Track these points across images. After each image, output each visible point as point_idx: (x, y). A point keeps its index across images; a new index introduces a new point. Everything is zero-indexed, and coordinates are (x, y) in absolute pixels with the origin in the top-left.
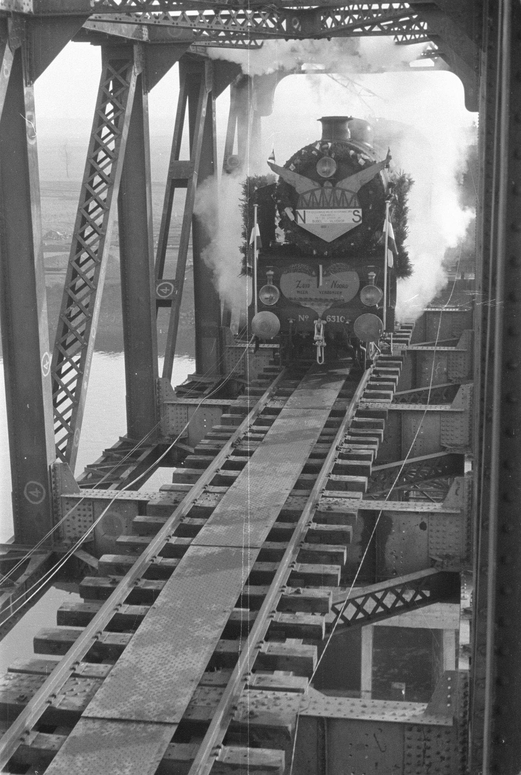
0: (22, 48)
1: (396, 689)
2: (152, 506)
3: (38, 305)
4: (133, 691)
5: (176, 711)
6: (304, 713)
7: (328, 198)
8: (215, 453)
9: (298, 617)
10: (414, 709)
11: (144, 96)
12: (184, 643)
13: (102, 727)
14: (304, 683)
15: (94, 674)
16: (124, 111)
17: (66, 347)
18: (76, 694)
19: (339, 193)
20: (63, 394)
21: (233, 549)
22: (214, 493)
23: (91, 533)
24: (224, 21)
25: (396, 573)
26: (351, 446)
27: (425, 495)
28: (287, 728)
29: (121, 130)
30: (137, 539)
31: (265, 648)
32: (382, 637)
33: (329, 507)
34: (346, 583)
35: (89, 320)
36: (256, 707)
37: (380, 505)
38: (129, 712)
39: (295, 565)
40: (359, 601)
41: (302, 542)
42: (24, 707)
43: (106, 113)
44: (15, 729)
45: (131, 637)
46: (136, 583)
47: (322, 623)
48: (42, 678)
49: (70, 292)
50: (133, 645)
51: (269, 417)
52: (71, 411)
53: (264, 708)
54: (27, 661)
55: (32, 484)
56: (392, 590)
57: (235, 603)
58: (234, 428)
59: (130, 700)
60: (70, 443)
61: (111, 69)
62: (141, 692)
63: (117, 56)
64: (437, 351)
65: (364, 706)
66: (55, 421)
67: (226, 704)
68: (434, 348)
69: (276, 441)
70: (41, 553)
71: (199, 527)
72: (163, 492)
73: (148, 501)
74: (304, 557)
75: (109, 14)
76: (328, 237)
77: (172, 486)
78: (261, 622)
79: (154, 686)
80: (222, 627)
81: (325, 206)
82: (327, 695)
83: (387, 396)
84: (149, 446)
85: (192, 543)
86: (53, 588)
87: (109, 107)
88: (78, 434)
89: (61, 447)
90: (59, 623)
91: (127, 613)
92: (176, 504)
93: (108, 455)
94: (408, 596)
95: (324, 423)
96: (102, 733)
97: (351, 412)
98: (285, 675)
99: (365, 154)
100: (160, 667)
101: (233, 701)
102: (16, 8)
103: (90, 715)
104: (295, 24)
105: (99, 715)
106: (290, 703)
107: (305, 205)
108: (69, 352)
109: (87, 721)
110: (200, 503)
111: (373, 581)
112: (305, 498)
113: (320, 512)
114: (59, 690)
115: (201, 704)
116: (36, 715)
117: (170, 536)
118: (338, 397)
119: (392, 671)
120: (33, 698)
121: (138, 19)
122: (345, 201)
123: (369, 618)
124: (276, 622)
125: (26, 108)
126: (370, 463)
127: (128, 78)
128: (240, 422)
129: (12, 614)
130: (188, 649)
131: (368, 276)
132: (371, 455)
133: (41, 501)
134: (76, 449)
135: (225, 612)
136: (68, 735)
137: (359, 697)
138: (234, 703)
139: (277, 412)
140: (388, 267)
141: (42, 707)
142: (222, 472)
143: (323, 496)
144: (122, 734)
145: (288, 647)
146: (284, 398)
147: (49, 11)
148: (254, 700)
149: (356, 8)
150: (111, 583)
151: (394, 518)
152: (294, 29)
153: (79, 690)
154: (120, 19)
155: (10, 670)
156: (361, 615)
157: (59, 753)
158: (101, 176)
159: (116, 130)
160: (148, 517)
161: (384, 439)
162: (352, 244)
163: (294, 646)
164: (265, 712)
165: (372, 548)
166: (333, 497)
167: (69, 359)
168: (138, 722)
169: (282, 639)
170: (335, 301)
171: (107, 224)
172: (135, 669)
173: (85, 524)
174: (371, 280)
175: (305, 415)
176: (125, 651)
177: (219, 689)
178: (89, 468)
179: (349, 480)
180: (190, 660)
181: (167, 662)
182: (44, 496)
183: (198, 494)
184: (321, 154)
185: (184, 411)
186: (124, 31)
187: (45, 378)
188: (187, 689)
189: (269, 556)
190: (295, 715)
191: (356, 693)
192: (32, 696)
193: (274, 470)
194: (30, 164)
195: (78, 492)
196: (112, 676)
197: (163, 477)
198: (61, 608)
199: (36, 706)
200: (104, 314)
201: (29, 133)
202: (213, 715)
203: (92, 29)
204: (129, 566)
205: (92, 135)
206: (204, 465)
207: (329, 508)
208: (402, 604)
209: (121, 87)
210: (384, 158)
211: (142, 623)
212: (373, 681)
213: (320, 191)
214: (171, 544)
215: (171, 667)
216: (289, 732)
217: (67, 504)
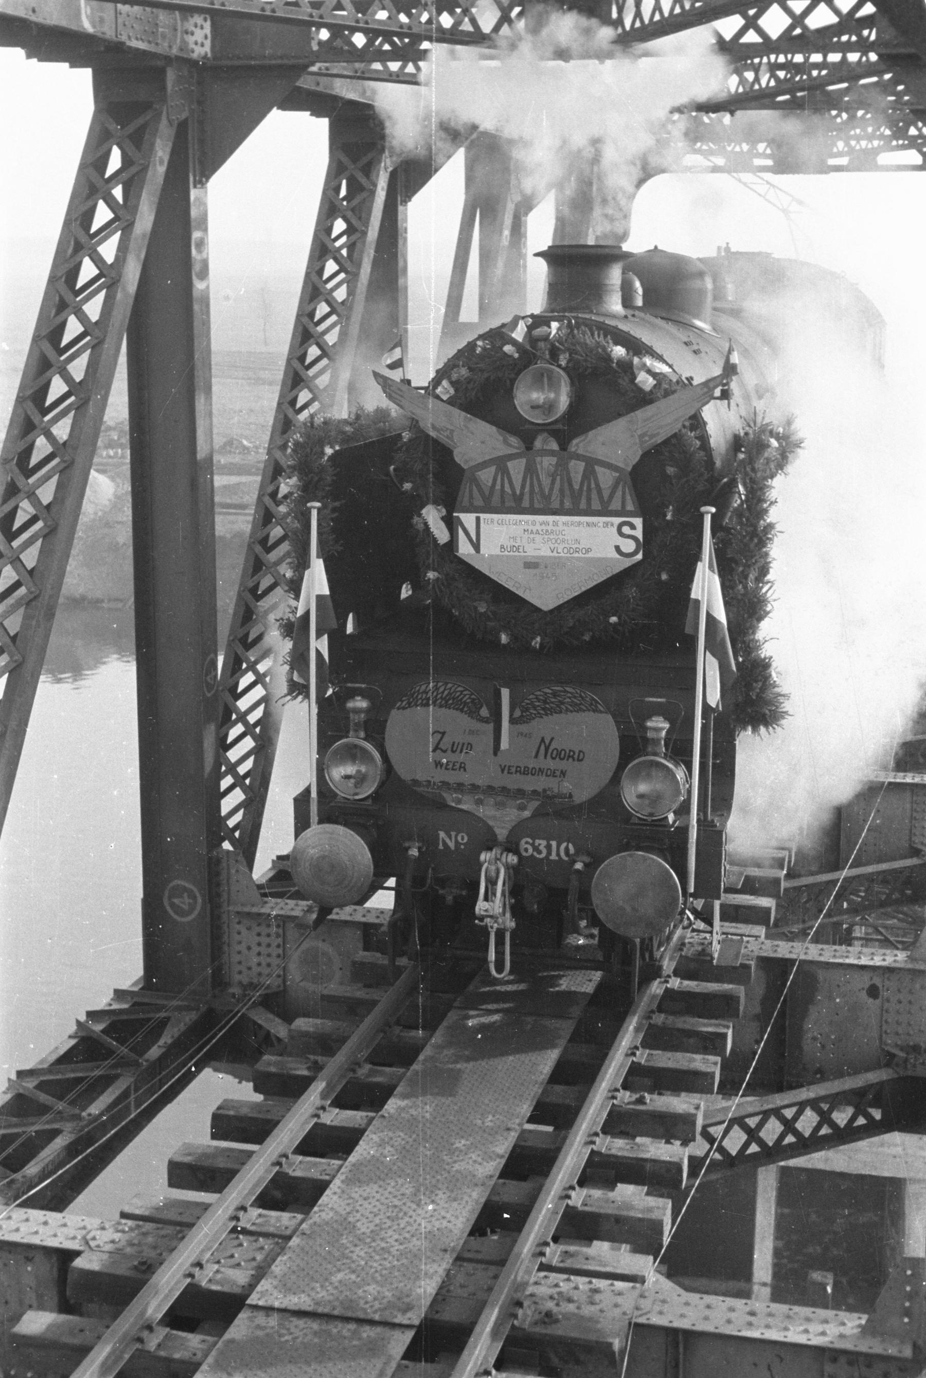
0: (190, 122)
1: (814, 1283)
7: (546, 481)
9: (638, 1145)
10: (844, 1324)
11: (400, 208)
12: (434, 1181)
14: (646, 1265)
15: (271, 1230)
16: (365, 233)
18: (239, 1265)
19: (577, 468)
25: (821, 1075)
27: (881, 934)
28: (610, 1345)
29: (359, 266)
31: (578, 1198)
32: (792, 1188)
33: (703, 950)
34: (729, 1087)
36: (557, 1305)
38: (330, 1301)
39: (638, 1053)
40: (752, 1122)
42: (144, 1282)
43: (334, 235)
44: (126, 1322)
45: (341, 1167)
46: (354, 1071)
47: (682, 1159)
48: (180, 1232)
49: (258, 549)
50: (343, 1182)
52: (252, 758)
53: (571, 1307)
56: (814, 1104)
61: (345, 160)
62: (353, 1266)
65: (752, 1314)
67: (503, 1297)
70: (188, 1008)
74: (655, 1038)
76: (546, 596)
79: (377, 1257)
80: (502, 1157)
81: (537, 505)
82: (688, 1289)
87: (339, 226)
90: (214, 1137)
94: (841, 1117)
96: (280, 1336)
98: (613, 1249)
99: (661, 358)
100: (389, 1223)
101: (516, 1291)
102: (181, 50)
103: (261, 1303)
105: (277, 1304)
106: (619, 1300)
107: (479, 502)
109: (255, 1314)
116: (167, 1297)
119: (810, 1250)
120: (163, 1267)
122: (594, 495)
123: (770, 1154)
124: (599, 1153)
125: (193, 224)
127: (373, 177)
129: (132, 1116)
130: (440, 1193)
131: (646, 729)
135: (508, 1129)
136: (220, 1335)
138: (518, 1295)
140: (706, 707)
141: (176, 1284)
144: (316, 1340)
147: (239, 58)
149: (782, 59)
150: (309, 1068)
151: (821, 975)
155: (124, 1215)
156: (754, 1148)
157: (204, 1367)
159: (348, 265)
162: (614, 619)
163: (630, 1197)
164: (574, 1314)
165: (780, 1028)
167: (252, 667)
169: (611, 1186)
170: (546, 797)
172: (344, 1225)
174: (656, 742)
176: (328, 1192)
177: (493, 1268)
179: (745, 903)
180: (443, 1213)
181: (401, 1215)
184: (529, 354)
188: (435, 1266)
191: (742, 1285)
192: (161, 1264)
194: (197, 323)
196: (304, 1234)
198: (219, 1108)
199: (168, 1282)
201: (196, 268)
205: (308, 275)
208: (830, 1131)
210: (717, 371)
211: (361, 1142)
213: (524, 460)
216: (614, 1353)
217: (239, 923)
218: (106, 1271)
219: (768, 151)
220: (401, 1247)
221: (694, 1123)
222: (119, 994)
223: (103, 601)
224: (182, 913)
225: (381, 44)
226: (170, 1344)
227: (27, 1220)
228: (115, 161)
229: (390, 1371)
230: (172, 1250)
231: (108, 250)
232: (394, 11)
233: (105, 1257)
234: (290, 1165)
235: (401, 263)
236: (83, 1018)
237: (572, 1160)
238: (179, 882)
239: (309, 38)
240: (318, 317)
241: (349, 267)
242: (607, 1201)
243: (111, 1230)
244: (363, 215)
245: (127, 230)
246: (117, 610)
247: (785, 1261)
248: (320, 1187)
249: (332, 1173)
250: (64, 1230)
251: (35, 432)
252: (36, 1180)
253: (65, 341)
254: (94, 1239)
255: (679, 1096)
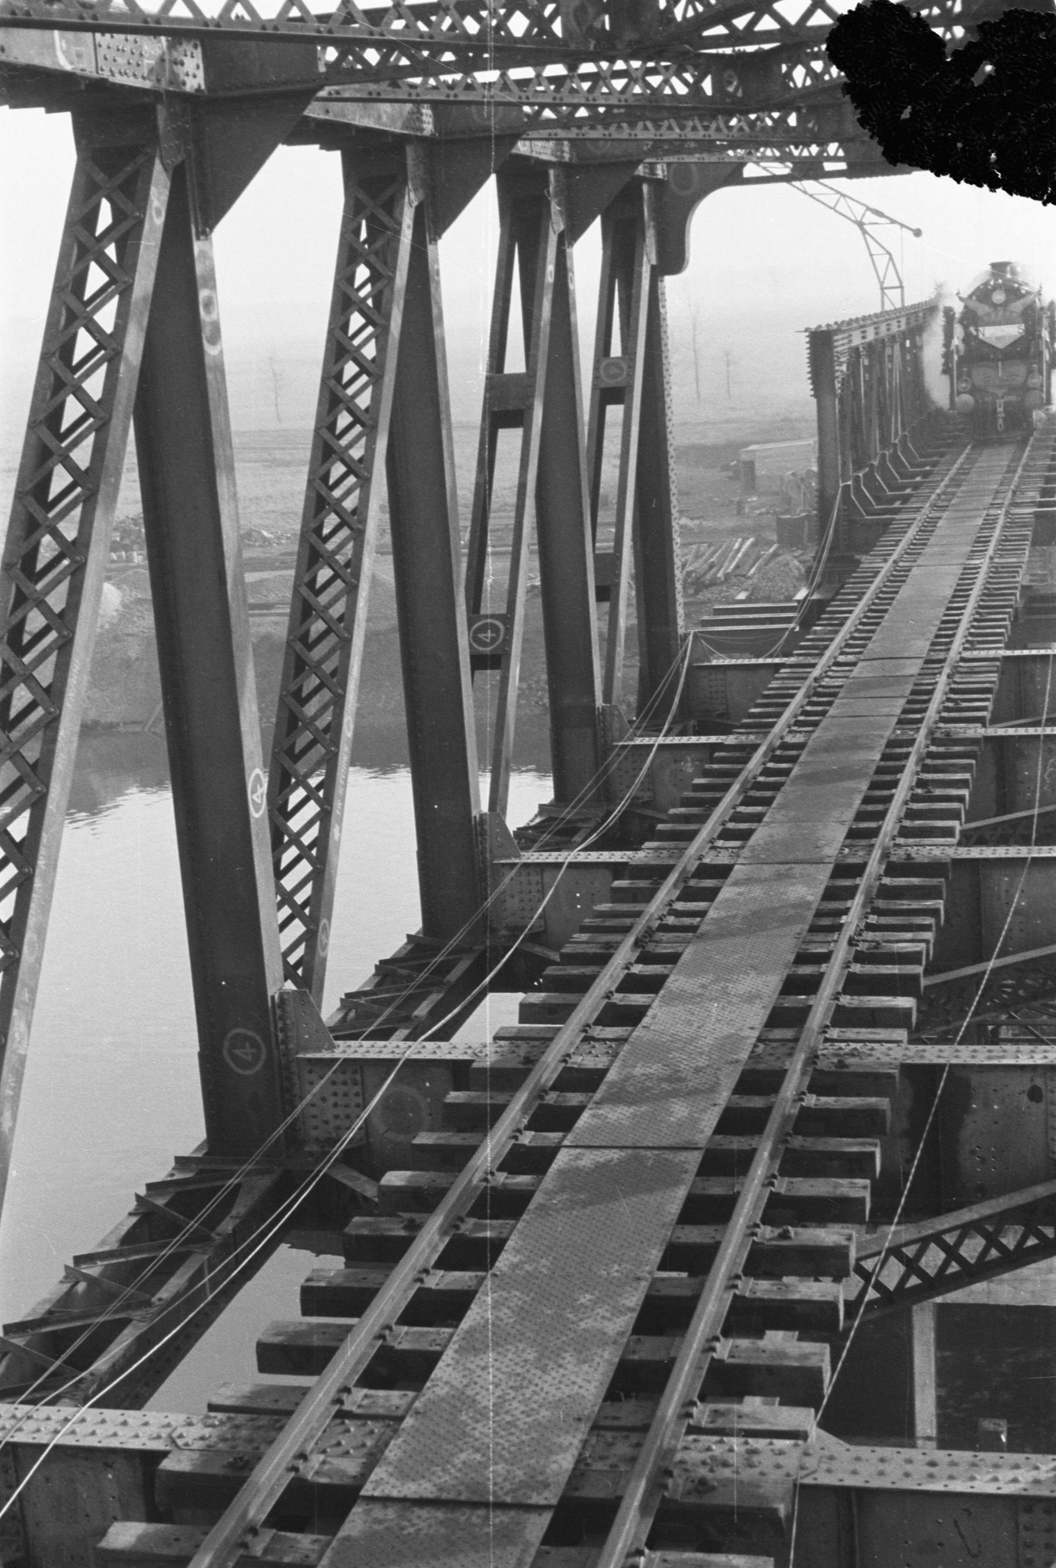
2: (482, 1071)
3: (238, 675)
4: (460, 1443)
5: (551, 1480)
6: (808, 1481)
8: (602, 960)
9: (787, 1286)
10: (1037, 1468)
11: (430, 247)
13: (401, 1517)
14: (804, 1418)
15: (381, 1411)
16: (392, 280)
17: (296, 758)
18: (347, 1453)
20: (292, 852)
21: (649, 1153)
22: (604, 1040)
23: (360, 1129)
24: (586, 85)
25: (983, 1193)
26: (878, 936)
27: (1032, 1033)
28: (775, 1511)
29: (388, 317)
30: (455, 1139)
31: (723, 1350)
33: (840, 1061)
34: (882, 1215)
35: (338, 702)
37: (945, 1054)
40: (910, 1251)
41: (788, 1134)
42: (242, 1481)
44: (227, 1526)
45: (452, 1335)
46: (457, 1227)
48: (278, 1421)
49: (299, 647)
50: (456, 1352)
51: (708, 883)
53: (727, 1473)
54: (247, 1389)
55: (238, 1035)
57: (658, 1260)
58: (638, 907)
59: (456, 1461)
60: (311, 950)
63: (374, 172)
64: (1047, 736)
65: (933, 1464)
66: (280, 906)
67: (650, 1465)
68: (1039, 731)
69: (725, 931)
71: (578, 1111)
72: (502, 1043)
73: (472, 1061)
74: (793, 1163)
75: (357, 86)
77: (520, 1029)
78: (713, 1297)
79: (503, 1433)
83: (948, 832)
84: (469, 951)
85: (566, 1143)
86: (284, 1247)
87: (362, 273)
88: (326, 930)
89: (292, 959)
90: (305, 1312)
91: (441, 1287)
92: (529, 1066)
93: (386, 970)
95: (820, 890)
96: (403, 1529)
97: (874, 866)
98: (765, 1403)
100: (512, 1393)
103: (377, 1494)
104: (730, 83)
105: (395, 1493)
106: (781, 1460)
108: (301, 767)
110: (578, 1061)
111: (938, 1211)
112: (791, 1045)
113: (822, 1072)
114: (312, 1444)
115: (599, 1466)
116: (270, 1494)
117: (519, 1131)
118: (847, 837)
119: (977, 1395)
120: (262, 1463)
121: (414, 92)
125: (200, 281)
126: (919, 969)
127: (397, 214)
128: (648, 895)
129: (210, 1297)
130: (567, 1355)
132: (920, 953)
133: (259, 1067)
134: (324, 960)
135: (639, 1279)
136: (334, 1534)
137: (913, 1446)
139: (723, 872)
141: (278, 1480)
142: (618, 998)
143: (826, 1040)
144: (443, 1530)
145: (770, 1347)
146: (737, 843)
148: (705, 1456)
150: (405, 1228)
151: (975, 1079)
152: (729, 94)
153: (354, 1444)
154: (379, 94)
155: (212, 1408)
156: (914, 1281)
158: (351, 412)
159: (376, 317)
160: (472, 1093)
161: (946, 920)
163: (780, 1344)
166: (847, 1041)
168: (474, 1505)
171: (366, 507)
172: (461, 1400)
173: (348, 1111)
175: (780, 877)
176: (440, 1364)
178: (350, 1000)
180: (573, 1378)
181: (525, 1383)
182: (263, 1057)
183: (572, 1044)
185: (535, 878)
186: (385, 117)
187: (257, 820)
188: (569, 1438)
189: (724, 1163)
190: (791, 1485)
192: (259, 1459)
193: (725, 992)
195: (331, 1048)
196: (417, 1413)
197: (497, 1013)
198: (308, 1280)
199: (269, 1479)
200: (367, 692)
202: (625, 1487)
203: (322, 116)
204: (440, 1193)
206: (583, 985)
207: (841, 1064)
209: (384, 232)
211: (473, 1306)
212: (939, 1416)
214: (523, 1146)
215: (535, 1393)
216: (779, 1518)
217: (310, 1072)
218: (199, 1470)
219: (841, 153)
220: (528, 1420)
221: (846, 1256)
222: (182, 1162)
223: (118, 725)
224: (245, 1065)
225: (398, 59)
226: (278, 1547)
227: (103, 1421)
228: (105, 217)
229: (529, 1560)
230: (271, 1442)
231: (106, 317)
232: (412, 18)
233: (196, 1455)
234: (396, 1337)
235: (435, 311)
236: (142, 1192)
237: (713, 1306)
238: (239, 1030)
239: (314, 59)
240: (346, 378)
241: (377, 317)
242: (757, 1350)
243: (200, 1425)
244: (389, 259)
245: (125, 294)
246: (134, 733)
247: (949, 1411)
248: (431, 1359)
249: (443, 1343)
250: (146, 1428)
251: (40, 531)
252: (107, 1377)
253: (65, 425)
254: (181, 1436)
255: (825, 1227)
